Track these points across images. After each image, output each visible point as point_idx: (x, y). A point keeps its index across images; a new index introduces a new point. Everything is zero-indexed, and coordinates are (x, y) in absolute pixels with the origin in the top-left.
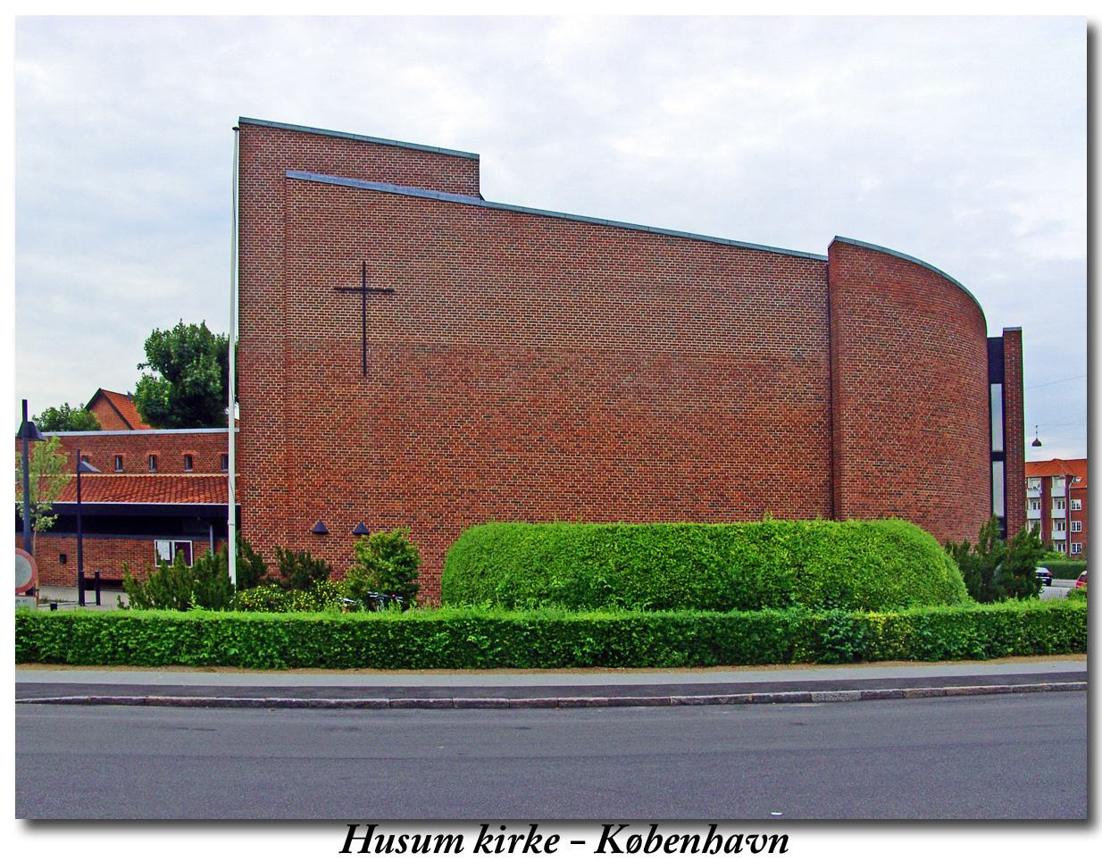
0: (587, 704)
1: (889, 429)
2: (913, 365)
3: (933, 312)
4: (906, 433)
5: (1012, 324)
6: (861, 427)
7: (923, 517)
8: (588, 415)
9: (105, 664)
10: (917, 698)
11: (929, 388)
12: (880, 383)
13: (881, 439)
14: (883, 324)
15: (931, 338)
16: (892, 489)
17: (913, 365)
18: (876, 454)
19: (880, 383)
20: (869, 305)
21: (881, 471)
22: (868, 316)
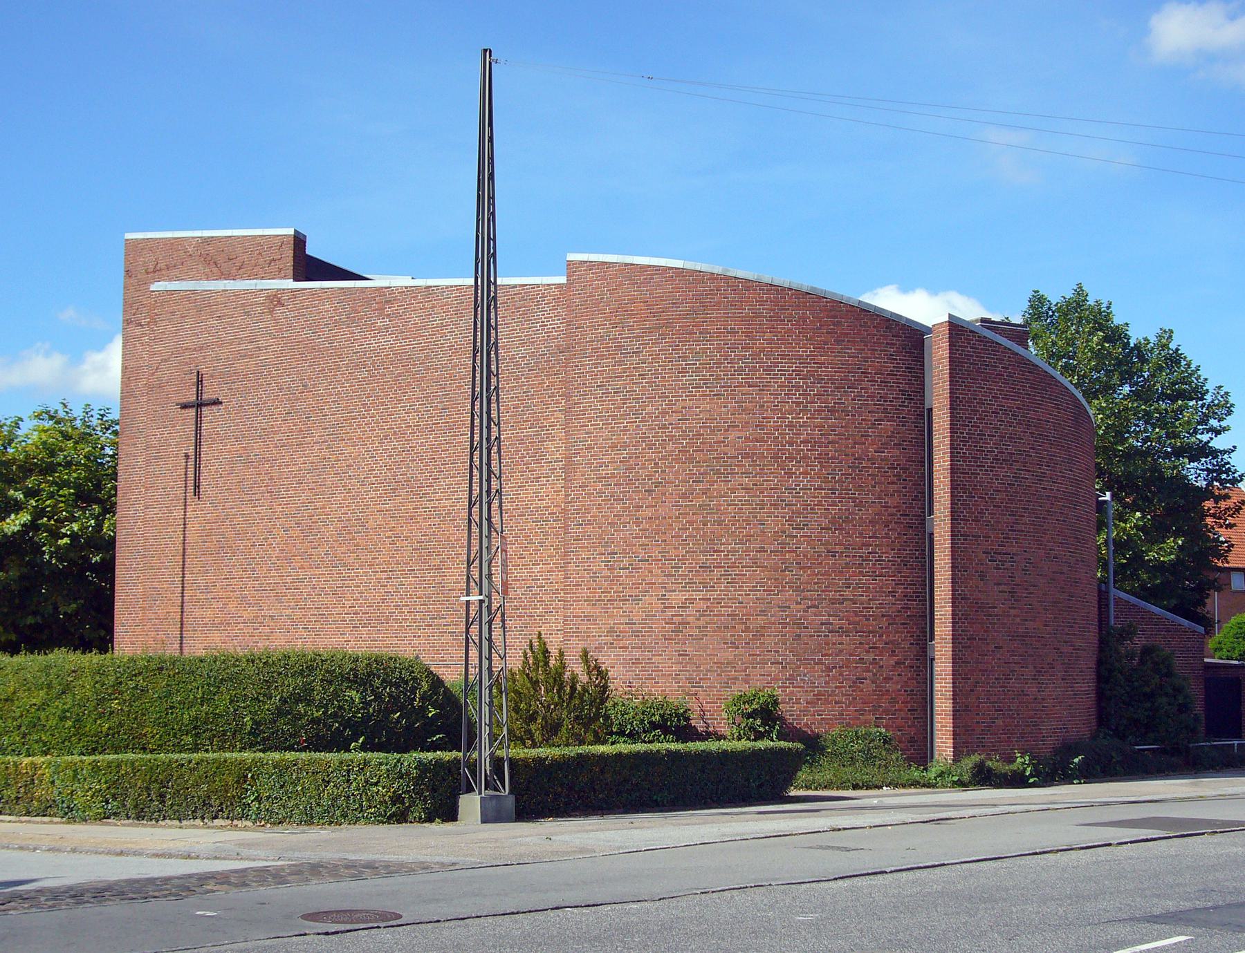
0: (324, 871)
1: (625, 509)
2: (664, 413)
3: (706, 332)
4: (649, 512)
5: (1030, 295)
6: (588, 511)
7: (677, 631)
8: (367, 520)
9: (139, 817)
10: (355, 877)
11: (691, 444)
12: (613, 446)
13: (612, 524)
14: (620, 363)
15: (697, 371)
16: (627, 593)
17: (664, 413)
18: (606, 546)
19: (613, 446)
20: (603, 339)
21: (611, 569)
22: (601, 357)
